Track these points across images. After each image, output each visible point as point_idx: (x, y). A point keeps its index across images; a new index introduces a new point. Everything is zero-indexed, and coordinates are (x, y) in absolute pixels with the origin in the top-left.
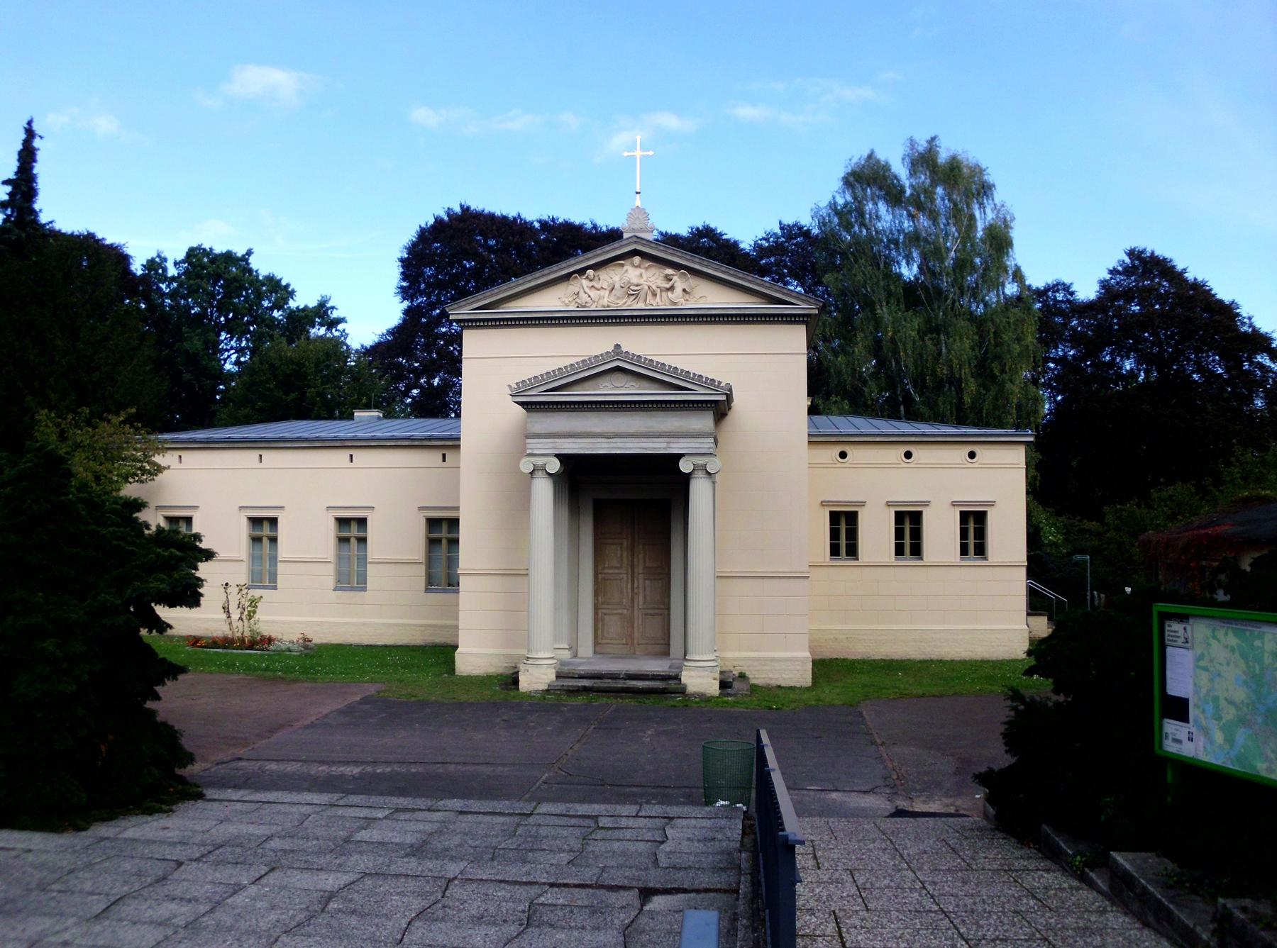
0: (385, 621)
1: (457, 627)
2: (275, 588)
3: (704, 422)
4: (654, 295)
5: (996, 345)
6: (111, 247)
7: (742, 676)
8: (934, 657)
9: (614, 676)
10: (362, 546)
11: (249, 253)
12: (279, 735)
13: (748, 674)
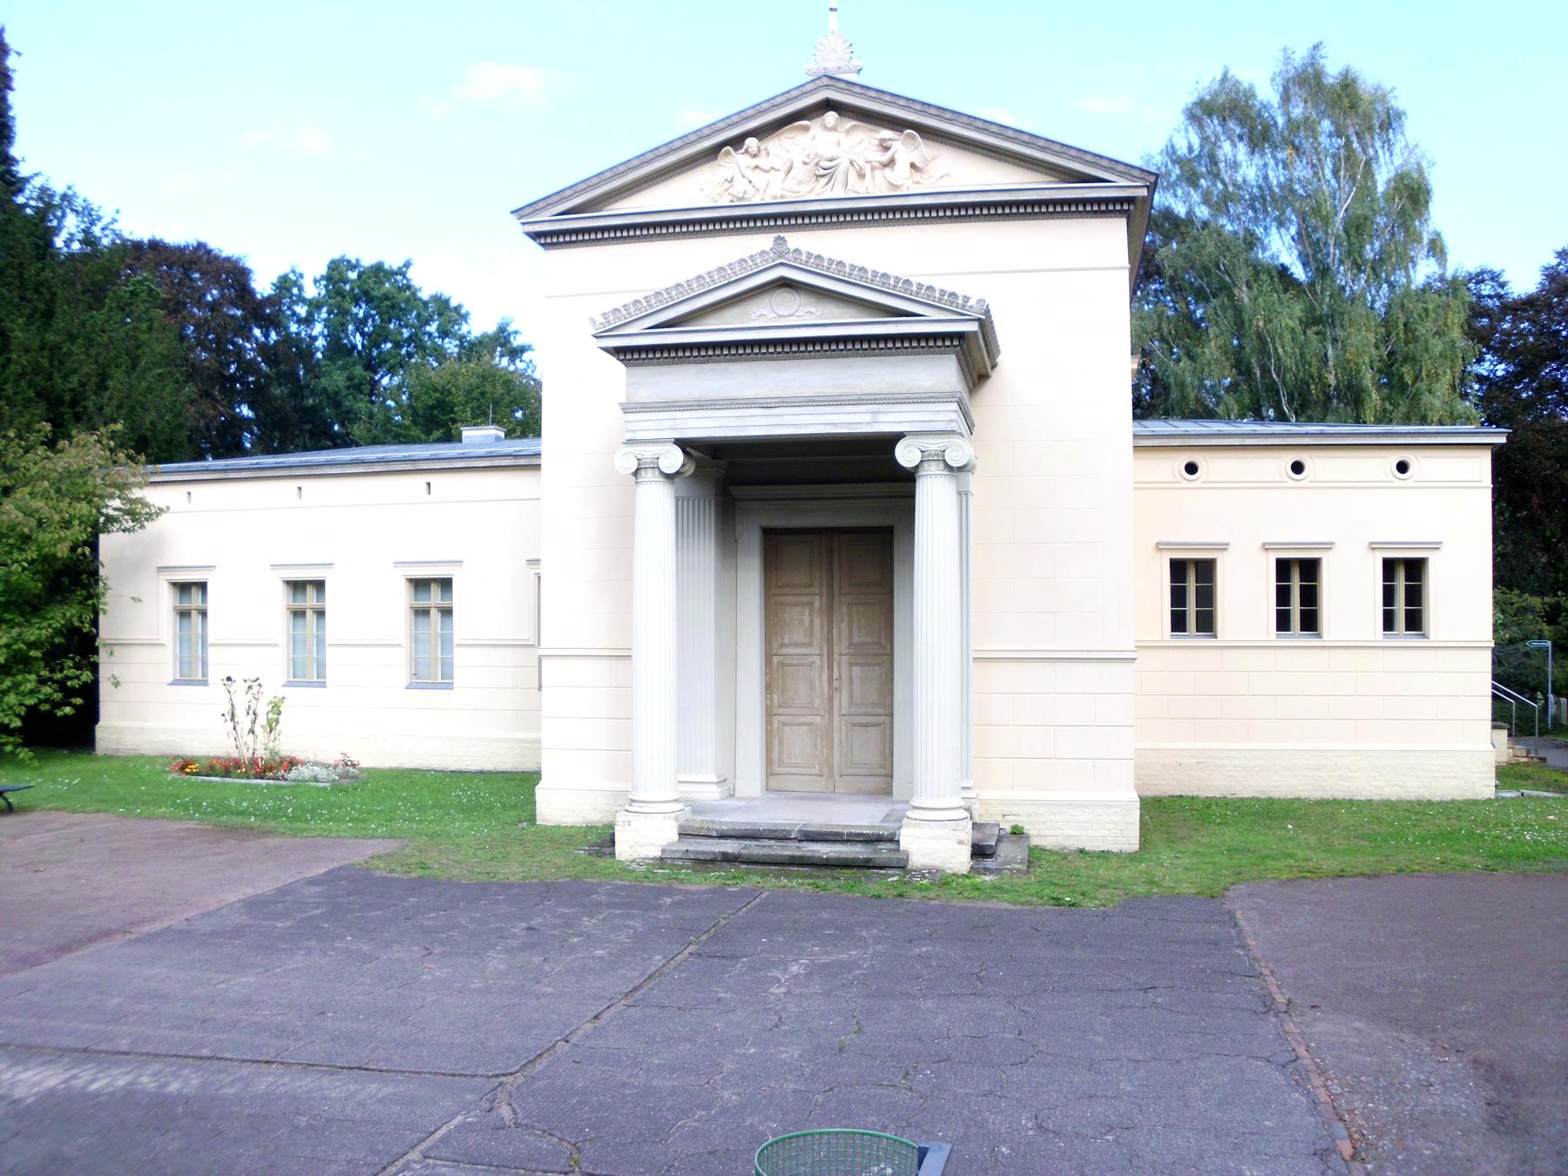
0: (521, 735)
1: (539, 741)
2: (323, 685)
3: (943, 372)
4: (862, 176)
5: (1407, 343)
6: (228, 259)
7: (1017, 833)
8: (1339, 795)
9: (781, 836)
10: (447, 619)
11: (407, 265)
12: (75, 963)
13: (1027, 828)
